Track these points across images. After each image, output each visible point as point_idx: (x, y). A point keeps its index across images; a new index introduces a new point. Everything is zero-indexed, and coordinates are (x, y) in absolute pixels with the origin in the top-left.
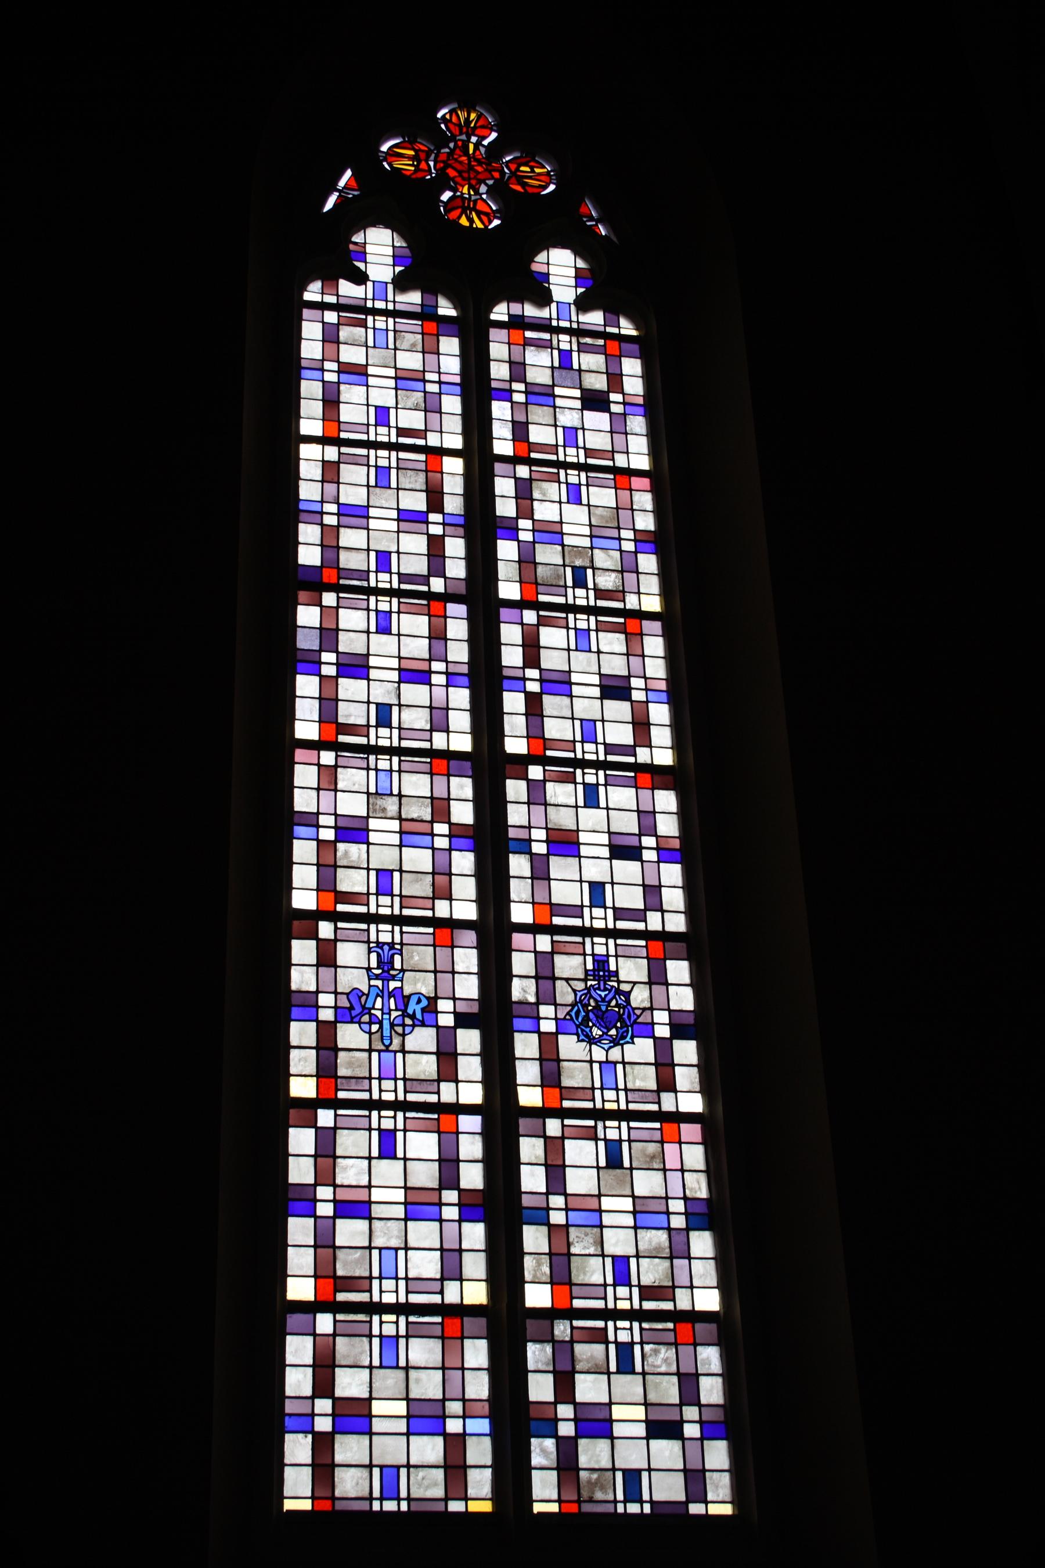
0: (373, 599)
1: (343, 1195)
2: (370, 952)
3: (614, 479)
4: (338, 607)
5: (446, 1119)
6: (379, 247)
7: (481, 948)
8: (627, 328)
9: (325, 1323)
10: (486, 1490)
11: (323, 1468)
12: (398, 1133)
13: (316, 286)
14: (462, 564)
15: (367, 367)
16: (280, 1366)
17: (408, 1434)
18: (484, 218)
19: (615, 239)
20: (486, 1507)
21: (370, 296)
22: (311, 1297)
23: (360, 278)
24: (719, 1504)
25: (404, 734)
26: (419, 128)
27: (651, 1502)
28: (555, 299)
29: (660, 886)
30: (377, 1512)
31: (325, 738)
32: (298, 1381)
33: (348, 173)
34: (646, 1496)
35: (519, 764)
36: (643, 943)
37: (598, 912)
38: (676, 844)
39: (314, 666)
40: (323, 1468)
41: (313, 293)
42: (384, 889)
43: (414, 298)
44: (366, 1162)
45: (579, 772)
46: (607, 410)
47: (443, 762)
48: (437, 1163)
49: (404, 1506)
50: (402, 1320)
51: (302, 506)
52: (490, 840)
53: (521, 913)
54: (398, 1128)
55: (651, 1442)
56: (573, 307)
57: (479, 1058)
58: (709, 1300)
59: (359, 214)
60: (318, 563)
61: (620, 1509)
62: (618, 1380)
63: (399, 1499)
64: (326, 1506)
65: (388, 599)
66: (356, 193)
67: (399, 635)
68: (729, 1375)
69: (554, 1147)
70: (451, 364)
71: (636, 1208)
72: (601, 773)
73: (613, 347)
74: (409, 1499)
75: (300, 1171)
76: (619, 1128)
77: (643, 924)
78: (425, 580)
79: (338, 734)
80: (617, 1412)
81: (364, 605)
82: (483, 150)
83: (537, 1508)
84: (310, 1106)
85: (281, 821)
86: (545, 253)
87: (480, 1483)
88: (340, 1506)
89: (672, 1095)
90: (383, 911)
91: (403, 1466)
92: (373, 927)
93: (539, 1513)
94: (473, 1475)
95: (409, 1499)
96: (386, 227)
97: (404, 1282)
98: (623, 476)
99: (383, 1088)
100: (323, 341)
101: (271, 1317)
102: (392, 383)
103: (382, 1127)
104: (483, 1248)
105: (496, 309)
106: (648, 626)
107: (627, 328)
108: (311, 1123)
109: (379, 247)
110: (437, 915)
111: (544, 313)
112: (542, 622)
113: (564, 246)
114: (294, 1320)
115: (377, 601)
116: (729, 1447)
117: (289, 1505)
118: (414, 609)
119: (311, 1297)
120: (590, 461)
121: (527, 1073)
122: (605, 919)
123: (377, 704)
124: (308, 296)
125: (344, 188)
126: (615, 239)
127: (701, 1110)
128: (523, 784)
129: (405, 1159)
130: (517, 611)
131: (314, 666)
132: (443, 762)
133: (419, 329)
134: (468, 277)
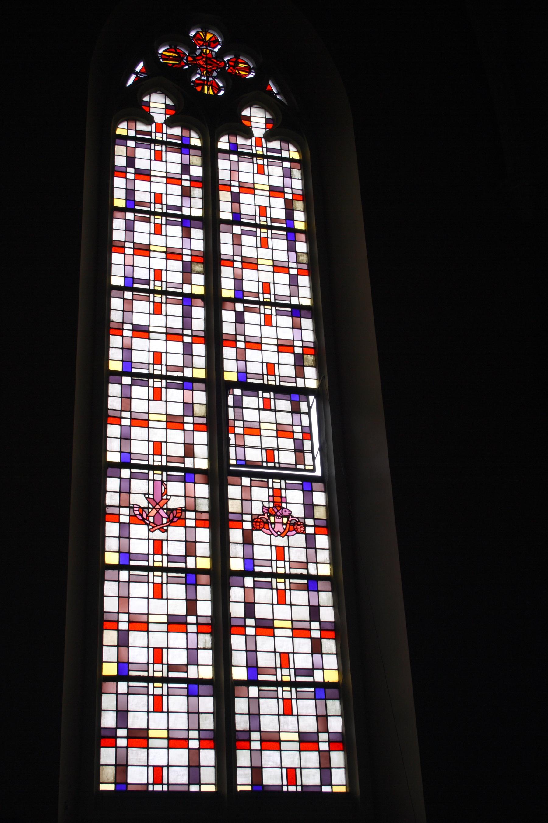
3: (287, 235)
4: (133, 300)
6: (158, 104)
8: (295, 155)
10: (212, 780)
13: (124, 125)
15: (151, 168)
17: (166, 429)
18: (215, 88)
19: (285, 102)
20: (212, 788)
22: (120, 369)
26: (179, 38)
27: (302, 785)
28: (254, 135)
30: (150, 791)
33: (141, 65)
34: (299, 783)
38: (300, 193)
39: (118, 420)
41: (122, 129)
43: (177, 131)
50: (283, 482)
52: (214, 340)
54: (164, 694)
56: (263, 140)
57: (210, 602)
58: (325, 570)
59: (146, 86)
61: (285, 789)
63: (297, 786)
65: (160, 217)
66: (145, 75)
67: (167, 599)
69: (254, 702)
70: (198, 245)
74: (168, 784)
75: (114, 403)
76: (291, 691)
77: (312, 678)
82: (213, 54)
83: (240, 788)
84: (120, 374)
86: (248, 109)
88: (130, 788)
91: (165, 540)
92: (151, 685)
93: (240, 791)
95: (168, 784)
98: (312, 583)
100: (125, 230)
101: (93, 684)
102: (164, 255)
103: (155, 693)
104: (214, 782)
106: (315, 485)
107: (295, 155)
109: (158, 104)
111: (248, 142)
114: (110, 471)
115: (154, 474)
117: (103, 787)
120: (273, 224)
122: (285, 567)
124: (119, 132)
125: (140, 72)
126: (285, 102)
130: (230, 226)
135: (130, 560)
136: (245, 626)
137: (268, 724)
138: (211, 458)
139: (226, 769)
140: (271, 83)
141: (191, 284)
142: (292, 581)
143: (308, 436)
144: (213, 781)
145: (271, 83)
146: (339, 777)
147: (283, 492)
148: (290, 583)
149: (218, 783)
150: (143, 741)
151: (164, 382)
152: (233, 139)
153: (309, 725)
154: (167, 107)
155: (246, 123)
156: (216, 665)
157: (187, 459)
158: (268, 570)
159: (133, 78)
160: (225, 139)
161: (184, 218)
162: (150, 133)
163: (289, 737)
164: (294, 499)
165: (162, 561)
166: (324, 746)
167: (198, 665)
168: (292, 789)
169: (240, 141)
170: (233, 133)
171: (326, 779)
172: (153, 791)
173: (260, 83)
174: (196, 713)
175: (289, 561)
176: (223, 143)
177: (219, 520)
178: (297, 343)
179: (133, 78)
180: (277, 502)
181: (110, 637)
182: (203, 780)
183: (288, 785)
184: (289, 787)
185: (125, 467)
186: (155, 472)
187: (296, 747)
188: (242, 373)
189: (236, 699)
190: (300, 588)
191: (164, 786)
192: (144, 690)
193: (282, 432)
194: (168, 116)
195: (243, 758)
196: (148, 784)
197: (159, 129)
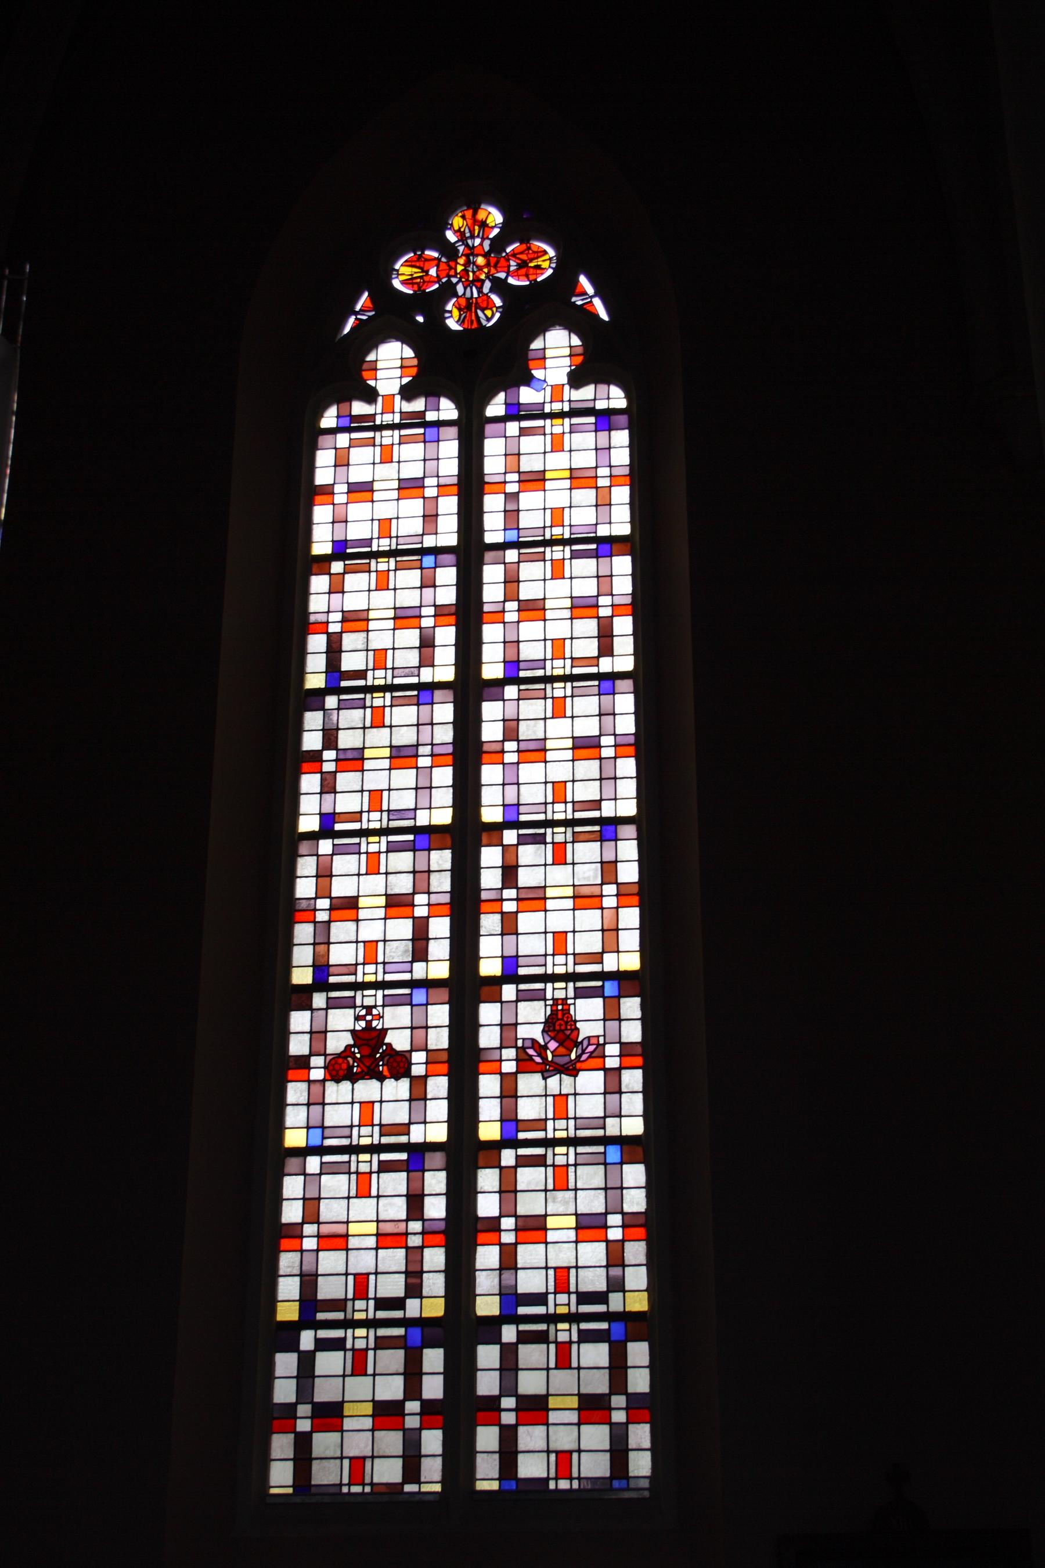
1: (325, 1229)
2: (546, 1005)
6: (391, 361)
10: (438, 1476)
11: (508, 1453)
15: (375, 477)
21: (548, 399)
23: (370, 395)
36: (596, 683)
40: (508, 1453)
41: (329, 419)
42: (370, 959)
49: (368, 1489)
50: (574, 1328)
59: (371, 335)
60: (343, 669)
61: (552, 1485)
63: (571, 1479)
65: (382, 695)
71: (574, 1227)
74: (579, 1478)
86: (541, 338)
87: (432, 1470)
94: (426, 1463)
95: (579, 1478)
96: (565, 328)
98: (608, 829)
105: (452, 406)
109: (391, 361)
113: (384, 341)
117: (482, 1486)
118: (406, 701)
136: (503, 752)
139: (459, 1457)
149: (446, 1479)
150: (368, 495)
151: (392, 561)
153: (593, 1203)
158: (539, 971)
159: (351, 321)
163: (563, 1413)
164: (588, 1014)
166: (615, 1234)
173: (563, 281)
175: (575, 1118)
177: (463, 1061)
179: (351, 321)
180: (560, 1023)
181: (303, 932)
182: (424, 1476)
185: (320, 990)
186: (375, 695)
188: (512, 808)
189: (481, 1077)
190: (588, 838)
192: (355, 849)
194: (405, 380)
195: (487, 1437)
197: (389, 409)
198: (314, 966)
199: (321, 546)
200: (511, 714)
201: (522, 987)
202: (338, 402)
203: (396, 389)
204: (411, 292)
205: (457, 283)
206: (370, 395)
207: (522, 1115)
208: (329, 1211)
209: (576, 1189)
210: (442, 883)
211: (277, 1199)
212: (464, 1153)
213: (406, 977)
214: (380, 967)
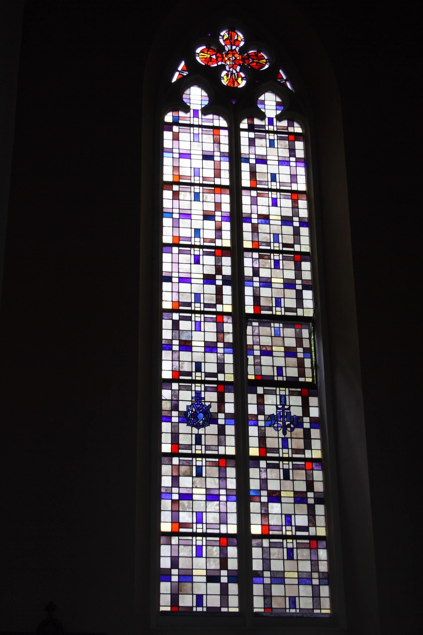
0: (192, 187)
5: (216, 131)
6: (196, 96)
7: (231, 195)
8: (298, 129)
9: (175, 386)
10: (328, 606)
12: (203, 547)
14: (228, 206)
15: (191, 147)
16: (160, 476)
20: (237, 610)
24: (326, 609)
25: (208, 526)
29: (297, 175)
31: (175, 242)
32: (166, 481)
33: (183, 63)
35: (256, 460)
36: (290, 194)
37: (285, 451)
39: (169, 419)
41: (169, 118)
42: (199, 469)
44: (191, 559)
45: (272, 255)
46: (295, 288)
47: (218, 188)
48: (219, 596)
51: (164, 210)
53: (247, 244)
54: (203, 465)
55: (285, 290)
62: (287, 563)
64: (176, 609)
65: (200, 385)
68: (325, 481)
72: (281, 255)
73: (292, 137)
78: (214, 306)
79: (179, 528)
80: (287, 575)
81: (189, 131)
85: (155, 494)
89: (310, 451)
90: (198, 378)
91: (289, 438)
92: (194, 538)
95: (300, 609)
97: (205, 525)
99: (198, 527)
101: (154, 538)
107: (298, 129)
108: (171, 130)
109: (196, 96)
110: (220, 453)
111: (188, 115)
112: (258, 195)
115: (195, 386)
116: (327, 551)
117: (162, 609)
119: (170, 451)
121: (254, 442)
123: (195, 294)
125: (182, 70)
127: (318, 416)
128: (255, 396)
129: (203, 265)
131: (169, 419)
132: (218, 188)
133: (212, 133)
134: (234, 106)
135: (179, 449)
137: (276, 566)
138: (235, 374)
139: (246, 597)
140: (281, 71)
141: (222, 239)
142: (207, 459)
143: (309, 355)
144: (237, 605)
145: (281, 71)
146: (326, 603)
147: (203, 393)
148: (206, 461)
152: (175, 114)
154: (278, 104)
155: (260, 106)
156: (239, 524)
157: (219, 375)
160: (245, 121)
161: (292, 192)
162: (264, 126)
163: (291, 576)
165: (201, 450)
167: (227, 524)
168: (200, 609)
169: (182, 114)
170: (176, 109)
171: (224, 601)
172: (196, 612)
173: (273, 72)
174: (190, 557)
176: (244, 125)
178: (174, 275)
183: (290, 609)
184: (198, 608)
186: (196, 385)
187: (297, 582)
191: (204, 608)
193: (290, 352)
195: (257, 589)
196: (193, 607)
198: (171, 594)
199: (167, 374)
200: (252, 149)
201: (272, 540)
202: (173, 111)
203: (199, 108)
204: (204, 64)
205: (227, 71)
206: (187, 109)
207: (268, 445)
208: (183, 564)
209: (297, 560)
210: (226, 208)
211: (158, 556)
212: (242, 462)
213: (217, 531)
214: (204, 525)
